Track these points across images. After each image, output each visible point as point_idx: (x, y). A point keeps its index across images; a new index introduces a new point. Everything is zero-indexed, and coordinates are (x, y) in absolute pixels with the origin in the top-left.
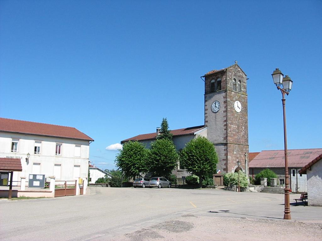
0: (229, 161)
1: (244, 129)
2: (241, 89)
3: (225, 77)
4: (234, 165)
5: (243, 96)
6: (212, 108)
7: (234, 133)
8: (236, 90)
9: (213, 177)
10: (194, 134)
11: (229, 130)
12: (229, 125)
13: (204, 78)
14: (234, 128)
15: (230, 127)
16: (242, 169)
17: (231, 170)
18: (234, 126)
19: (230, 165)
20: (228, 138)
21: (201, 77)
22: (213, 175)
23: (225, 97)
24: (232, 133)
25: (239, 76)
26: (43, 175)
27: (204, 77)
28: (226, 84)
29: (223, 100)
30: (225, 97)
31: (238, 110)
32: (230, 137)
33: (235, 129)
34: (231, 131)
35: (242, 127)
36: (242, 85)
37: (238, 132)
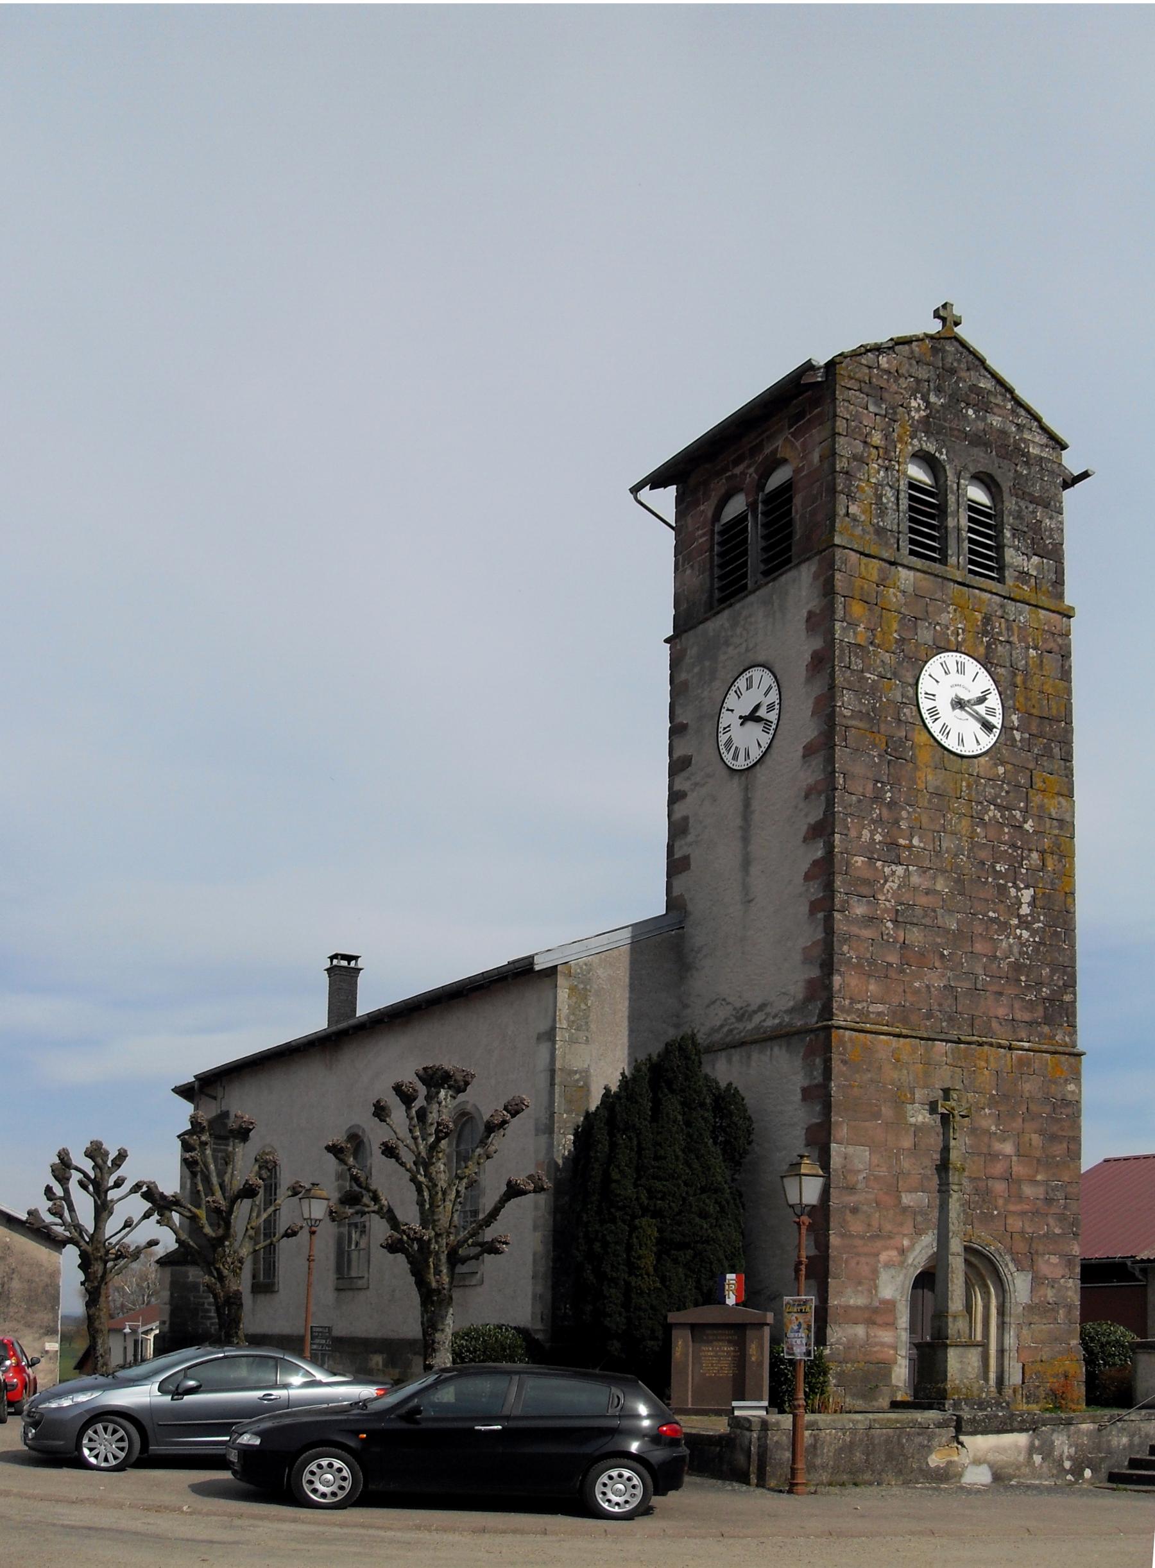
0: (851, 1189)
1: (1025, 910)
2: (1000, 559)
3: (826, 433)
4: (908, 1228)
5: (1023, 616)
6: (723, 739)
7: (915, 936)
8: (943, 561)
9: (675, 1333)
10: (532, 964)
11: (859, 909)
12: (859, 860)
13: (665, 499)
14: (907, 897)
15: (867, 882)
16: (1008, 1268)
17: (875, 1273)
18: (915, 879)
19: (856, 1226)
20: (837, 980)
21: (635, 490)
22: (672, 1318)
23: (821, 621)
24: (884, 942)
25: (978, 440)
26: (763, 1487)
27: (657, 480)
28: (833, 491)
29: (800, 647)
30: (821, 621)
31: (966, 736)
32: (871, 969)
33: (923, 900)
34: (871, 920)
35: (1002, 890)
36: (1009, 520)
37: (960, 937)
